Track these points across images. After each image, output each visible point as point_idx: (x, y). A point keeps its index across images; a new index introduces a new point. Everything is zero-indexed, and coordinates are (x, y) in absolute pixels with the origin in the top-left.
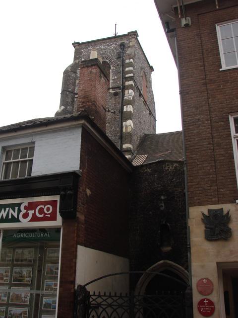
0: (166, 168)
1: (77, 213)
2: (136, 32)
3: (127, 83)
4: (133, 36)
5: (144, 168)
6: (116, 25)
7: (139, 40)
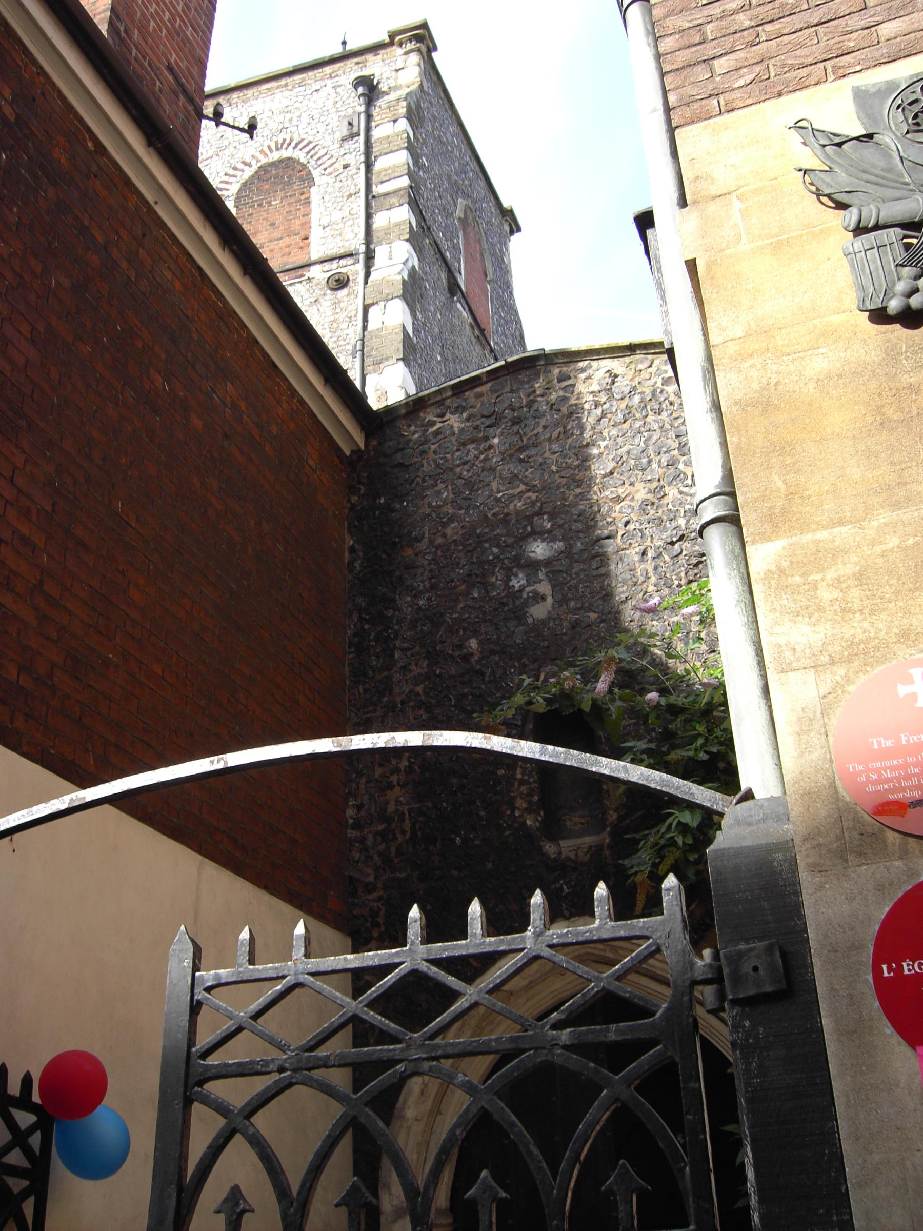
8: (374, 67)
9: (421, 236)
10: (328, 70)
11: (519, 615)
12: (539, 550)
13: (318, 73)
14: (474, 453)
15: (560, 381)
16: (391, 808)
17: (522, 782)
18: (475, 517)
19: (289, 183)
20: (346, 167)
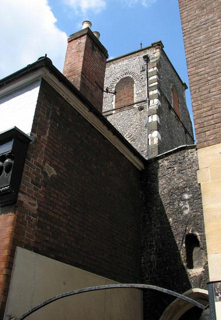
0: (190, 156)
1: (20, 194)
2: (160, 42)
3: (151, 93)
4: (157, 47)
5: (160, 161)
6: (141, 44)
7: (165, 51)
8: (149, 53)
9: (161, 97)
10: (137, 54)
11: (182, 213)
12: (186, 196)
13: (135, 55)
14: (170, 171)
15: (191, 153)
16: (152, 259)
17: (182, 254)
18: (171, 188)
19: (128, 83)
20: (142, 79)
